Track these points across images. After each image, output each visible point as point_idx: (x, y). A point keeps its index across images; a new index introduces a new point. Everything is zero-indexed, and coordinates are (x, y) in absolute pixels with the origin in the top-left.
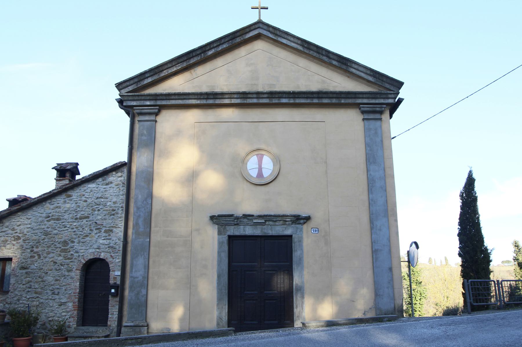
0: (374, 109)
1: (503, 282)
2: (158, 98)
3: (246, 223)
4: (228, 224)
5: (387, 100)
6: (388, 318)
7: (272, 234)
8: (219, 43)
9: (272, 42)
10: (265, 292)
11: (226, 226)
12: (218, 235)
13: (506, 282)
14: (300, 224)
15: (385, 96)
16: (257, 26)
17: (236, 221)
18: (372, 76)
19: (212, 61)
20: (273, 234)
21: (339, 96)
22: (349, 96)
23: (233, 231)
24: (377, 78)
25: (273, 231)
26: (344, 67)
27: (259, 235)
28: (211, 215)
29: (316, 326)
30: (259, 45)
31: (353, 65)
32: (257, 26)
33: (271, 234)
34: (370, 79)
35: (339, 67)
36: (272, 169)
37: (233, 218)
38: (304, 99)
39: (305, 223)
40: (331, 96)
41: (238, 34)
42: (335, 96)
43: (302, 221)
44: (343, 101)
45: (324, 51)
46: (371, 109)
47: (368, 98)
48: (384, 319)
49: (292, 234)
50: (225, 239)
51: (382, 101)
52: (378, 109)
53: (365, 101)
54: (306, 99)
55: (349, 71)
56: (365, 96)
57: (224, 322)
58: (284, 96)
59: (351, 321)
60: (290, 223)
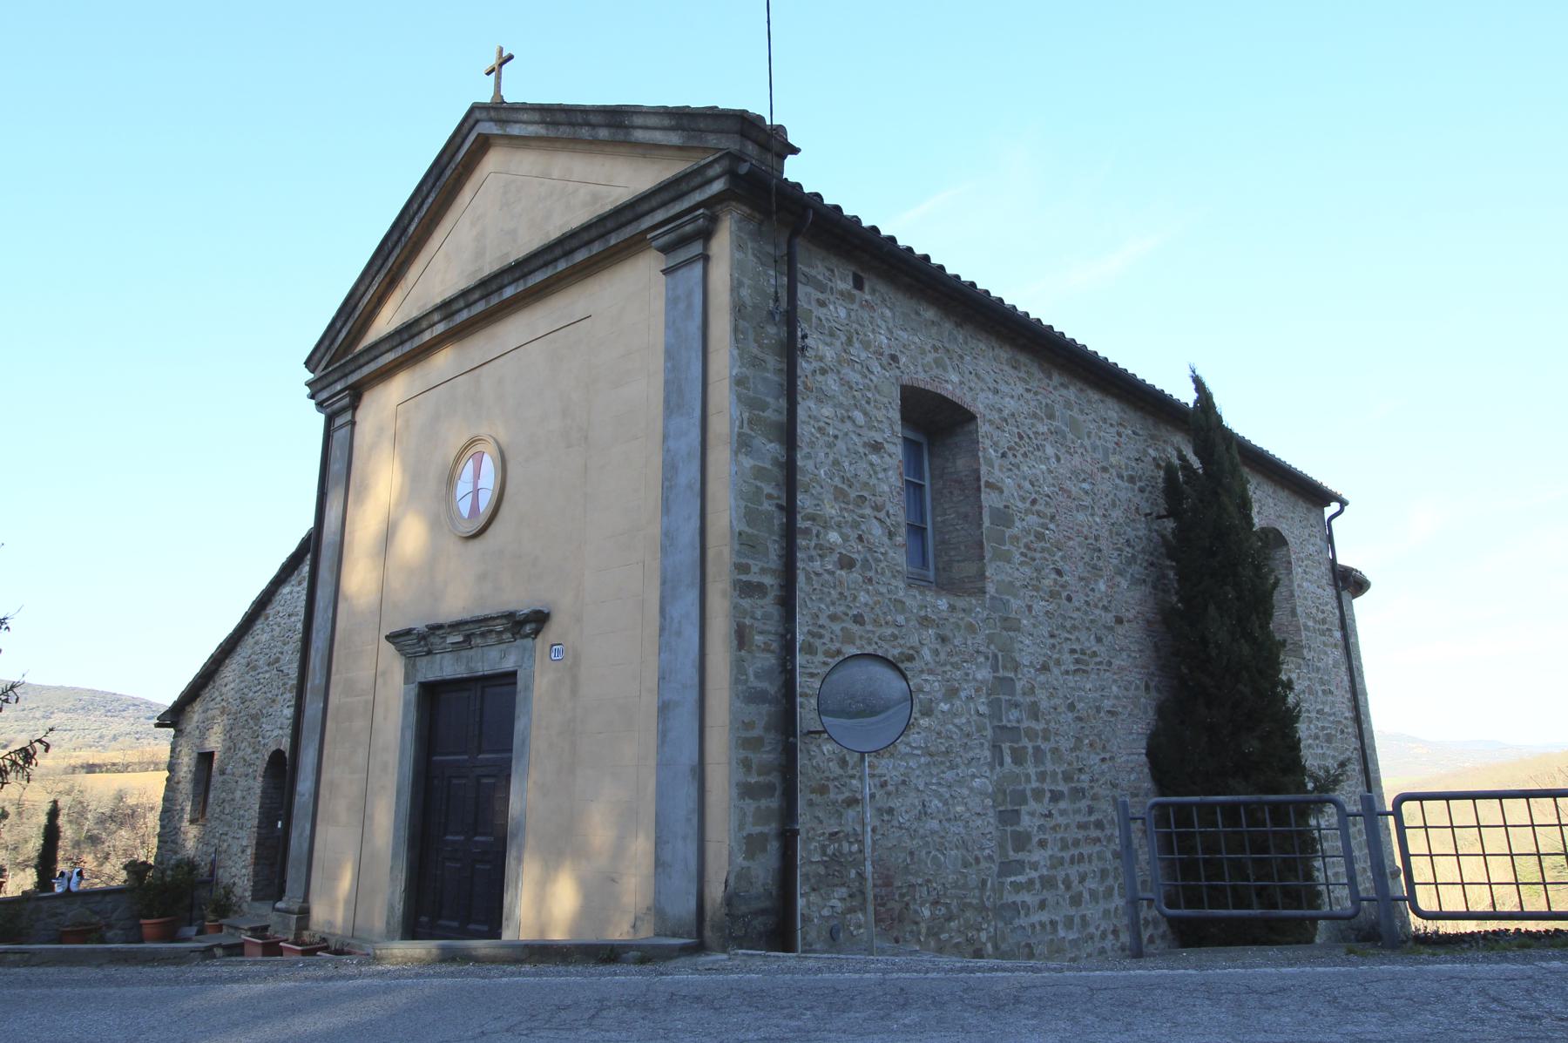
0: (679, 231)
1: (1409, 808)
2: (347, 371)
3: (440, 647)
4: (415, 653)
5: (707, 187)
6: (638, 951)
7: (483, 671)
8: (420, 199)
9: (507, 142)
10: (449, 838)
11: (418, 659)
12: (405, 684)
13: (1551, 800)
14: (527, 636)
15: (698, 180)
16: (471, 121)
17: (422, 643)
18: (678, 130)
19: (428, 243)
20: (486, 673)
21: (602, 230)
22: (623, 219)
23: (447, 667)
24: (687, 131)
25: (485, 664)
26: (620, 136)
27: (465, 675)
28: (552, 615)
29: (402, 957)
30: (493, 161)
31: (638, 121)
32: (471, 121)
33: (481, 673)
34: (674, 138)
35: (612, 141)
36: (492, 488)
37: (411, 637)
38: (541, 271)
39: (536, 632)
40: (586, 237)
41: (445, 159)
42: (594, 233)
43: (528, 628)
44: (614, 240)
45: (579, 113)
46: (673, 236)
47: (664, 204)
48: (627, 953)
49: (515, 668)
50: (413, 690)
51: (698, 197)
52: (688, 228)
53: (660, 216)
54: (544, 269)
55: (630, 142)
56: (654, 203)
57: (396, 920)
58: (506, 279)
59: (506, 950)
60: (509, 635)
